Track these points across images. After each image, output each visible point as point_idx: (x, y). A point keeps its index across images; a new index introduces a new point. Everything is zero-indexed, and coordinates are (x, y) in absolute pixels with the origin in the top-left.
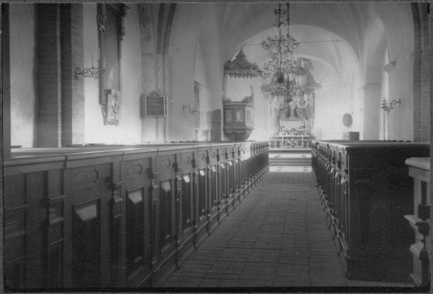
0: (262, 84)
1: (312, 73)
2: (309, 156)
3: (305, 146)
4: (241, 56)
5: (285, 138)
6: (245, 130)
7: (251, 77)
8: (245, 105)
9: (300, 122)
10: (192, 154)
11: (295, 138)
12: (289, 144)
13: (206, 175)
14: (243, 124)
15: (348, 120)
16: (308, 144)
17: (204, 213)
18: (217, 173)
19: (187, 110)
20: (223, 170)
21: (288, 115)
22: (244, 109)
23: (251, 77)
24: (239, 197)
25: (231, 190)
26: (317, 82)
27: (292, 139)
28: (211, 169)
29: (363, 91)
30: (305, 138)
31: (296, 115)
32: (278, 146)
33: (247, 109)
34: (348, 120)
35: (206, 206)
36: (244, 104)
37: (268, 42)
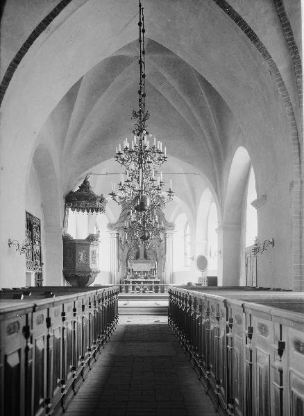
1: (163, 211)
3: (156, 292)
4: (85, 186)
5: (134, 282)
6: (90, 272)
7: (97, 211)
9: (150, 265)
12: (138, 289)
14: (87, 265)
15: (202, 263)
16: (160, 289)
17: (43, 405)
19: (14, 247)
20: (57, 343)
21: (137, 257)
23: (97, 211)
24: (82, 373)
26: (170, 220)
27: (142, 283)
29: (222, 231)
30: (155, 282)
31: (146, 257)
33: (91, 248)
34: (202, 263)
35: (45, 396)
36: (87, 243)
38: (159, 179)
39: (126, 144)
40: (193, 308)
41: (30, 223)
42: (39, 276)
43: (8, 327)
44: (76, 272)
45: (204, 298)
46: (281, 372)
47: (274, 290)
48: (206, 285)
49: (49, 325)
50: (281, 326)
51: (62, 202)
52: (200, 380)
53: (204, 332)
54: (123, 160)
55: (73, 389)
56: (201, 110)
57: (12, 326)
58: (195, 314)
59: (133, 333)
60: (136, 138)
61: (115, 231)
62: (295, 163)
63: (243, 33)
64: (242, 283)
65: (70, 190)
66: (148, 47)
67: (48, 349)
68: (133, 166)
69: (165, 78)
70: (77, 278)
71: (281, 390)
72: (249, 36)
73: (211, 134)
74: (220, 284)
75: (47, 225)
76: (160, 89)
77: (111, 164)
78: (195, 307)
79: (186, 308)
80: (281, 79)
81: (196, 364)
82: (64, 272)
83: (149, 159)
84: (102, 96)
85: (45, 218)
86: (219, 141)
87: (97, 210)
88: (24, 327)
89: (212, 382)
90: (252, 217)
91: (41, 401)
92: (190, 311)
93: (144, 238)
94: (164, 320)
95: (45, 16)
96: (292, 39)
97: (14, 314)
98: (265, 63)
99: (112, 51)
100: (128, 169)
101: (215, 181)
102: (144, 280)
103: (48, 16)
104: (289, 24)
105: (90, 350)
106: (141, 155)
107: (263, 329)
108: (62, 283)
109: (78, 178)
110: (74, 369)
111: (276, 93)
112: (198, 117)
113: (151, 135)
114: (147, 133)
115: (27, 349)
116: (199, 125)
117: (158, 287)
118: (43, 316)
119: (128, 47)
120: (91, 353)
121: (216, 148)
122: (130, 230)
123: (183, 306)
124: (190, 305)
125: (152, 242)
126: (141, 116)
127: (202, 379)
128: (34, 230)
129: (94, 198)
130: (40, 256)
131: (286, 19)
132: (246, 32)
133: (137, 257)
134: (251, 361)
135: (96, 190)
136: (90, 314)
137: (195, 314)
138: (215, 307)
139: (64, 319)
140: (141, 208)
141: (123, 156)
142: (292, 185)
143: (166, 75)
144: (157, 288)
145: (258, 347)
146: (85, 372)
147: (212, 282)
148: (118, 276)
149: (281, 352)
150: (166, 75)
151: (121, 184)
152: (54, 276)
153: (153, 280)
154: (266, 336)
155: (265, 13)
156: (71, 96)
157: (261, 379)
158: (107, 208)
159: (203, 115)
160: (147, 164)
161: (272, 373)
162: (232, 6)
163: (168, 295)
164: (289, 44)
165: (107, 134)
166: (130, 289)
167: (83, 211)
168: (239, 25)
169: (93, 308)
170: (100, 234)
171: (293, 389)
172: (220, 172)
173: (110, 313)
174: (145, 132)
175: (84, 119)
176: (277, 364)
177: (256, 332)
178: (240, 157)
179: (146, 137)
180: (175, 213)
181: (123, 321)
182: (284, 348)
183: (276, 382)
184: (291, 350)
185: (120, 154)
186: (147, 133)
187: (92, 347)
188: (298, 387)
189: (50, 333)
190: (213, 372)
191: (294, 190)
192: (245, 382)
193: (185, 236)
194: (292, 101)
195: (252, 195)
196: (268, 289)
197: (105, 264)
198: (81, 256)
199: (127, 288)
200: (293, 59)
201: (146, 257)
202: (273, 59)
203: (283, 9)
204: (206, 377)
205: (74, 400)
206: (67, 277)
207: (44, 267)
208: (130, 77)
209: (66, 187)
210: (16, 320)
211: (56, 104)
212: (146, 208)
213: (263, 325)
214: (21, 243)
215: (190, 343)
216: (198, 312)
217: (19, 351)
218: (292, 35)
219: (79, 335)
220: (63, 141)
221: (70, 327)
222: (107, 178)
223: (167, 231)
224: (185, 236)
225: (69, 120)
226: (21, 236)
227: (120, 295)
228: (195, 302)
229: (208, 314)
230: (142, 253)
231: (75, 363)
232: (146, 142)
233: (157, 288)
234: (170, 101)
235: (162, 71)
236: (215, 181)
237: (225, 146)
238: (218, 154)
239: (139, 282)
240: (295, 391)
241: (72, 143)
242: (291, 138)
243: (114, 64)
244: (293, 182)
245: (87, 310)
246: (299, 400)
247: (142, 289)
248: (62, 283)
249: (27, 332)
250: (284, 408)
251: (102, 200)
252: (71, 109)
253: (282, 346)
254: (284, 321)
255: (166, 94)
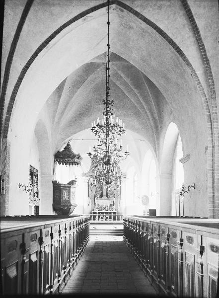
0: (82, 172)
2: (121, 227)
3: (114, 219)
4: (68, 148)
5: (99, 213)
8: (70, 187)
10: (21, 236)
11: (106, 213)
12: (102, 218)
13: (39, 260)
14: (69, 201)
15: (146, 200)
18: (50, 253)
20: (56, 249)
21: (102, 196)
22: (70, 189)
23: (75, 165)
24: (69, 272)
25: (64, 266)
27: (105, 214)
28: (44, 252)
31: (107, 196)
32: (94, 219)
34: (146, 200)
36: (69, 186)
37: (97, 129)
38: (119, 144)
39: (99, 121)
40: (141, 229)
41: (32, 173)
42: (37, 208)
43: (31, 237)
44: (61, 206)
45: (150, 222)
46: (202, 265)
47: (196, 218)
48: (148, 215)
49: (52, 238)
50: (202, 236)
51: (52, 159)
52: (146, 277)
53: (149, 245)
54: (96, 131)
55: (64, 281)
56: (145, 98)
57: (33, 236)
58: (143, 233)
59: (100, 248)
60: (105, 117)
61: (87, 179)
62: (209, 134)
63: (173, 50)
64: (173, 214)
65: (57, 150)
66: (112, 57)
67: (40, 261)
68: (103, 135)
69: (122, 77)
70: (62, 209)
71: (202, 276)
72: (178, 52)
73: (152, 114)
74: (158, 214)
75: (42, 174)
76: (118, 84)
77: (87, 133)
78: (143, 228)
79: (137, 229)
80: (199, 80)
81: (143, 266)
82: (53, 206)
83: (113, 131)
84: (80, 89)
85: (41, 169)
86: (157, 118)
87: (76, 163)
88: (21, 244)
89: (155, 277)
90: (179, 168)
91: (47, 286)
92: (139, 231)
93: (107, 183)
94: (121, 239)
95: (46, 38)
96: (205, 55)
97: (35, 229)
98: (188, 69)
99: (88, 59)
100: (99, 137)
101: (154, 141)
102: (106, 211)
103: (48, 38)
104: (203, 45)
105: (73, 257)
106: (108, 128)
107: (190, 240)
108: (51, 213)
109: (64, 142)
110: (65, 268)
111: (196, 89)
112: (143, 103)
113: (114, 116)
114: (112, 114)
115: (41, 251)
116: (144, 108)
117: (115, 216)
118: (48, 231)
119: (98, 57)
120: (75, 259)
121: (155, 123)
122: (98, 178)
123: (137, 229)
124: (139, 227)
125: (113, 185)
126: (107, 102)
127: (148, 276)
128: (34, 177)
129: (74, 156)
130: (38, 195)
131: (202, 42)
132: (176, 49)
133: (102, 196)
134: (182, 260)
135: (75, 150)
136: (74, 232)
137: (143, 233)
138: (157, 228)
139: (60, 235)
140: (108, 163)
141: (96, 129)
142: (207, 148)
143: (122, 75)
144: (114, 217)
145: (187, 251)
146: (71, 271)
147: (153, 213)
148: (88, 209)
149: (202, 253)
150: (122, 75)
151: (95, 147)
152: (47, 209)
153: (112, 212)
154: (192, 244)
155: (188, 38)
156: (60, 89)
157: (189, 273)
158: (82, 162)
159: (147, 101)
160: (112, 134)
161: (196, 265)
162: (166, 33)
163: (123, 222)
164: (204, 58)
165: (83, 113)
166: (97, 217)
167: (66, 164)
168: (171, 45)
169: (75, 229)
170: (77, 180)
171: (209, 275)
172: (158, 139)
173: (83, 235)
174: (110, 114)
175: (68, 103)
176: (200, 261)
177: (185, 242)
178: (171, 130)
179: (111, 116)
180: (125, 166)
181: (92, 239)
182: (204, 250)
183: (199, 272)
184: (207, 250)
185: (94, 127)
186: (112, 114)
187: (75, 255)
188: (214, 273)
189: (42, 249)
190: (156, 270)
191: (208, 151)
192: (179, 274)
193: (134, 181)
194: (206, 93)
195: (180, 154)
196: (192, 217)
197: (81, 202)
198: (65, 194)
199: (94, 217)
200: (206, 68)
201: (107, 196)
202: (194, 67)
203: (200, 36)
204: (151, 274)
205: (65, 288)
206: (55, 209)
207: (40, 202)
208: (99, 76)
209: (55, 149)
210: (35, 233)
211: (50, 94)
212: (111, 163)
213: (190, 237)
214: (27, 185)
215: (139, 253)
216: (145, 231)
217: (37, 252)
218: (206, 52)
219: (68, 246)
220: (54, 117)
221: (63, 240)
222: (84, 143)
223: (122, 179)
224: (134, 181)
225: (58, 104)
226: (27, 182)
227: (91, 222)
228: (144, 226)
229: (152, 233)
230: (105, 193)
231: (65, 265)
232: (111, 120)
233: (114, 217)
234: (125, 92)
235: (120, 72)
236: (154, 141)
237: (161, 122)
238: (157, 127)
239: (103, 213)
240: (212, 276)
241: (60, 119)
242: (206, 117)
243: (89, 68)
244: (207, 147)
245: (72, 230)
246: (213, 281)
247: (104, 218)
248: (51, 213)
249: (41, 241)
250: (204, 288)
251: (79, 157)
252: (60, 96)
253: (202, 248)
254: (204, 234)
255: (122, 87)
